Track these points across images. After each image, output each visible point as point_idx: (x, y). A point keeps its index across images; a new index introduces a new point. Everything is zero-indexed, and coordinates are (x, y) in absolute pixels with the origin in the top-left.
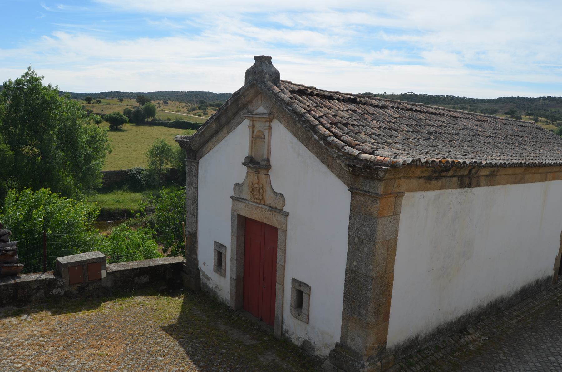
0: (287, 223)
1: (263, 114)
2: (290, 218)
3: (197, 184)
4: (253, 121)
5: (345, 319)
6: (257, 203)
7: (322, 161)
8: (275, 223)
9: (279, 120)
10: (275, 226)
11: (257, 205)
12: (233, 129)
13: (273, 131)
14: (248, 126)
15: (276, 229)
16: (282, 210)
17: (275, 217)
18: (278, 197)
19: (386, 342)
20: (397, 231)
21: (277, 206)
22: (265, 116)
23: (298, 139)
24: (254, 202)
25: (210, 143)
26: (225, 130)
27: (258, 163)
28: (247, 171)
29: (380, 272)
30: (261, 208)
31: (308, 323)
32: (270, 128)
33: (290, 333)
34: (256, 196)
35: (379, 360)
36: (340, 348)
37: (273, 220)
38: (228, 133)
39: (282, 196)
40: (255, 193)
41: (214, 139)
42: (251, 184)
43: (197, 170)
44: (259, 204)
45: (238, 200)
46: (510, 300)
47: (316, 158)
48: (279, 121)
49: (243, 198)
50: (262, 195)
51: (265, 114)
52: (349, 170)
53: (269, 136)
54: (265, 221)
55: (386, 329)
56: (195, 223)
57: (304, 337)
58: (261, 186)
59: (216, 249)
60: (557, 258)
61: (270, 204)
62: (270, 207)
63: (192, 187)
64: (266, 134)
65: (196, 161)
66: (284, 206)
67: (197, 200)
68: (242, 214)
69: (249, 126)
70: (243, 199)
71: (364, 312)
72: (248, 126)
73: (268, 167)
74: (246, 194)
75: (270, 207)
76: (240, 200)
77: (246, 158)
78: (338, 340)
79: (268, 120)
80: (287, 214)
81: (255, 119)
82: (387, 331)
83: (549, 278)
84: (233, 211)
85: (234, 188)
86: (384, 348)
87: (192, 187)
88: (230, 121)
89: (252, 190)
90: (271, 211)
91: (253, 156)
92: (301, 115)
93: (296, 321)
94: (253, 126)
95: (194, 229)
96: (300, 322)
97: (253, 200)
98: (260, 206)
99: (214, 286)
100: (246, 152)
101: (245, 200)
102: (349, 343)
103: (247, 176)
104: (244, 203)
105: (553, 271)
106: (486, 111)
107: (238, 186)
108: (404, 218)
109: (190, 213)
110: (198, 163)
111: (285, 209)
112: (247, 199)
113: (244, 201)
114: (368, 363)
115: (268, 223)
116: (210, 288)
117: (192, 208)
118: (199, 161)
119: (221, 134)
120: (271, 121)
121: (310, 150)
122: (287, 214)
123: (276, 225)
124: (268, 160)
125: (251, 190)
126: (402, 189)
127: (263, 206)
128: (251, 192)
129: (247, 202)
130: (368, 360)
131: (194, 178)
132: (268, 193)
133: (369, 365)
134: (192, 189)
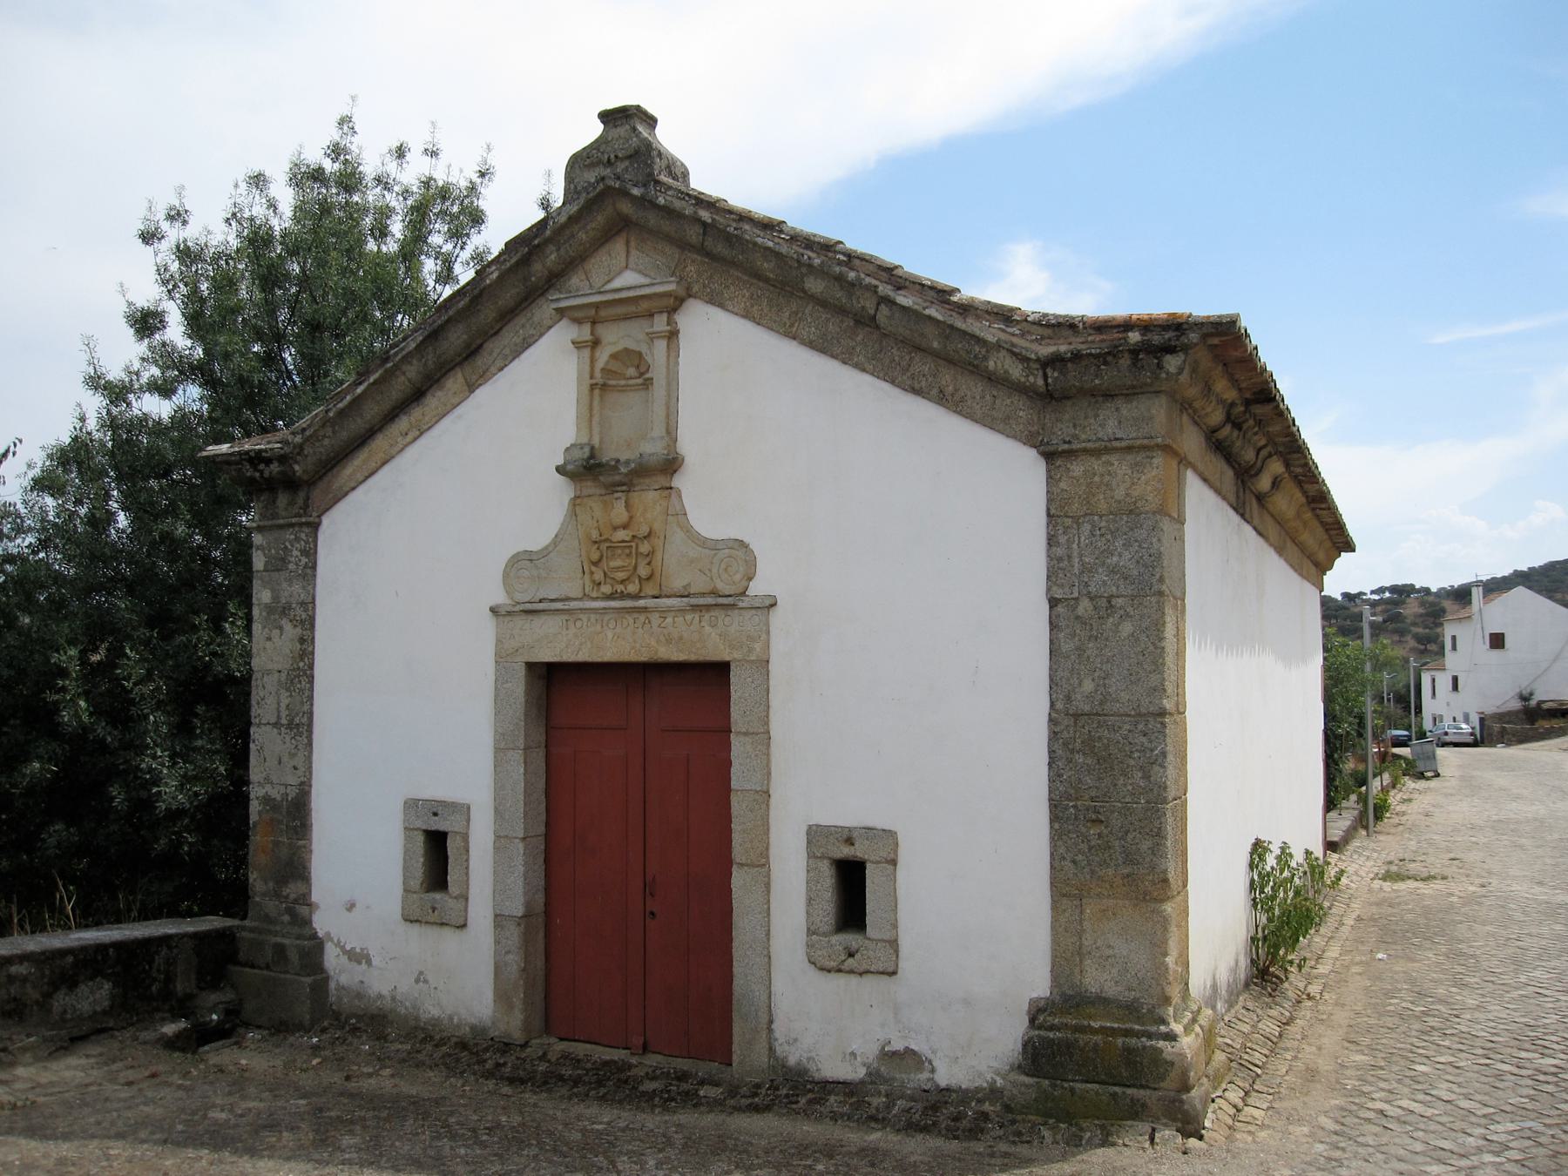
3: (309, 605)
12: (493, 369)
38: (472, 388)
41: (403, 423)
66: (750, 579)
88: (480, 346)
98: (642, 603)
110: (315, 526)
117: (285, 702)
118: (319, 516)
119: (433, 401)
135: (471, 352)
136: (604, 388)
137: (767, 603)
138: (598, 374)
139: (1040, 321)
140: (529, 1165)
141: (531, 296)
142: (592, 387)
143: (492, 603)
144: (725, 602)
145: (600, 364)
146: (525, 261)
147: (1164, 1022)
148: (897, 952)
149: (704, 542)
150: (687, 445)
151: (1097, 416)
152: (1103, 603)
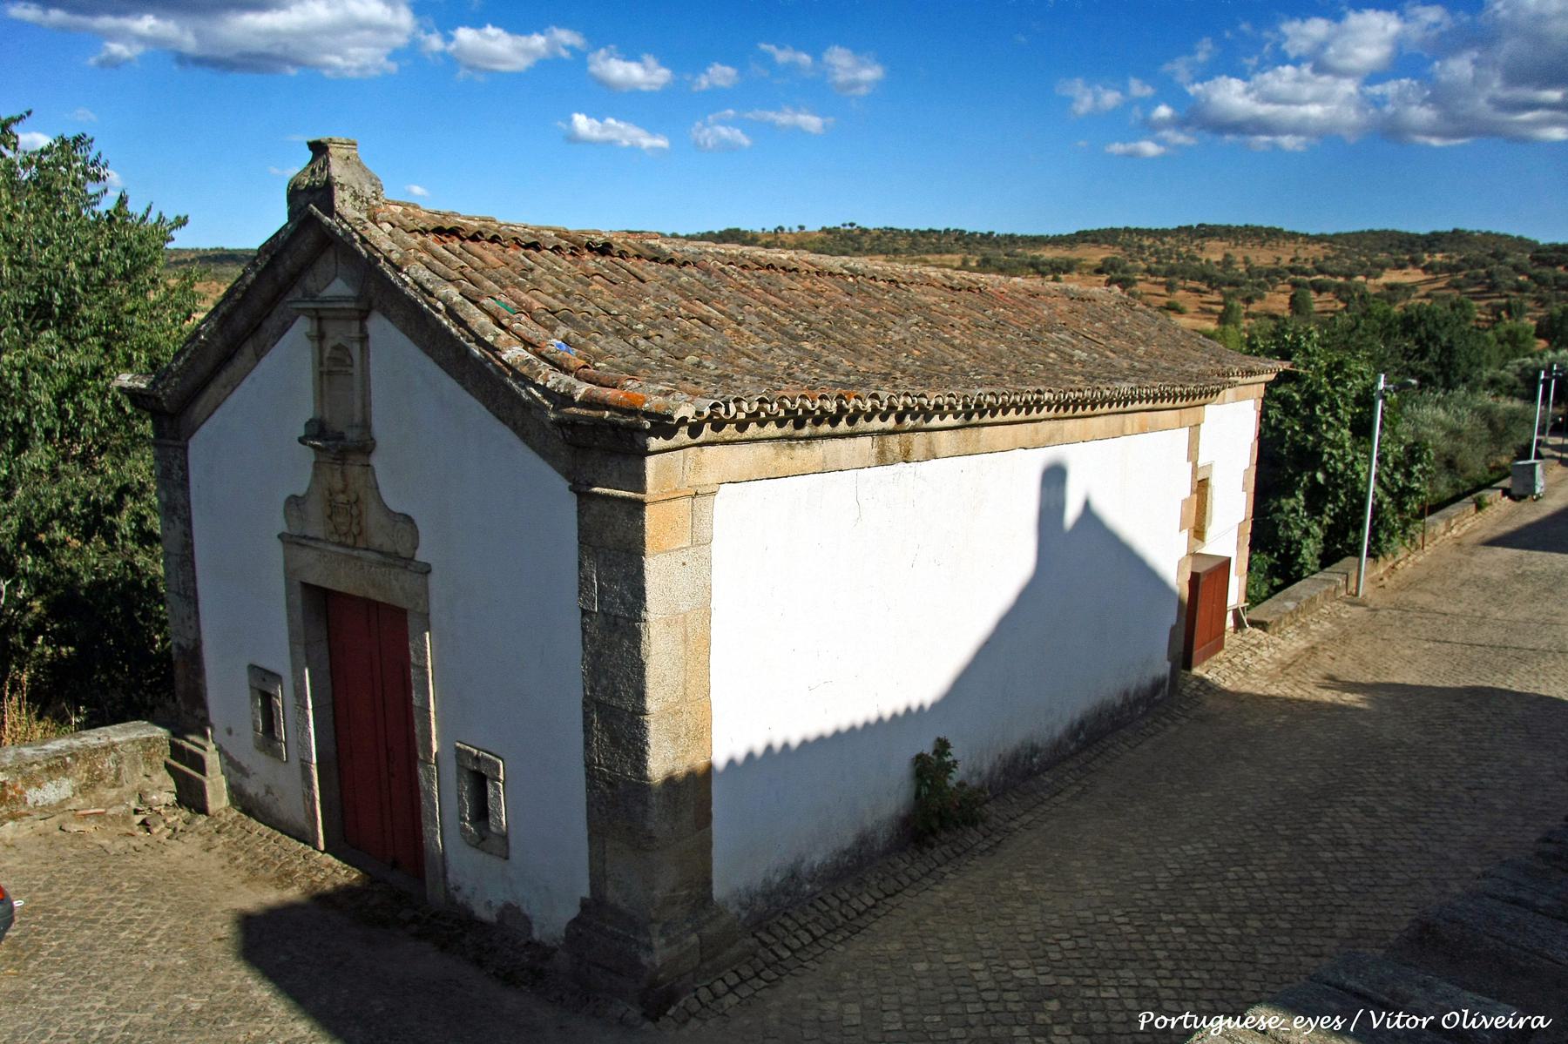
0: (427, 593)
1: (339, 299)
2: (434, 580)
3: (187, 506)
4: (320, 319)
5: (597, 833)
6: (348, 546)
7: (499, 417)
8: (398, 599)
9: (386, 313)
10: (399, 605)
11: (348, 551)
12: (269, 344)
13: (373, 345)
14: (306, 334)
15: (403, 612)
16: (412, 559)
17: (397, 580)
18: (400, 525)
19: (708, 883)
20: (708, 588)
21: (399, 550)
22: (346, 305)
23: (435, 361)
24: (340, 544)
25: (213, 391)
26: (248, 350)
27: (341, 437)
28: (313, 459)
29: (670, 700)
30: (358, 558)
31: (507, 858)
32: (364, 339)
33: (467, 891)
34: (344, 528)
35: (693, 930)
36: (593, 907)
37: (393, 588)
38: (258, 357)
39: (408, 519)
40: (340, 520)
41: (223, 378)
42: (327, 493)
43: (184, 468)
44: (354, 547)
45: (298, 544)
46: (1058, 746)
47: (483, 408)
48: (384, 315)
49: (311, 535)
50: (359, 523)
51: (346, 299)
52: (563, 434)
53: (362, 358)
54: (374, 594)
55: (706, 847)
56: (194, 618)
57: (499, 897)
58: (353, 498)
59: (256, 685)
60: (1173, 629)
61: (381, 545)
62: (381, 553)
63: (175, 518)
64: (356, 349)
65: (180, 443)
66: (416, 548)
67: (192, 554)
68: (312, 581)
69: (309, 337)
70: (311, 539)
71: (639, 808)
72: (306, 334)
73: (366, 448)
74: (316, 529)
75: (381, 553)
76: (304, 541)
77: (307, 425)
78: (585, 892)
79: (356, 314)
80: (426, 570)
81: (322, 314)
82: (710, 853)
83: (1157, 685)
84: (289, 574)
85: (285, 511)
86: (706, 899)
87: (175, 518)
88: (260, 324)
89: (332, 510)
90: (384, 564)
91: (327, 416)
92: (259, 275)
93: (479, 857)
94: (320, 337)
95: (191, 635)
96: (488, 857)
97: (336, 538)
98: (355, 553)
99: (262, 792)
100: (307, 411)
101: (317, 539)
102: (612, 895)
103: (315, 475)
104: (316, 549)
105: (1168, 665)
106: (1232, 289)
107: (294, 502)
108: (722, 550)
109: (178, 594)
110: (185, 449)
111: (421, 556)
112: (321, 536)
113: (312, 543)
114: (663, 941)
115: (380, 599)
116: (250, 797)
117: (181, 578)
118: (187, 441)
119: (239, 363)
120: (364, 316)
121: (467, 389)
122: (426, 570)
123: (402, 603)
124: (366, 425)
125: (328, 512)
126: (709, 477)
127: (362, 553)
128: (330, 517)
129: (321, 545)
130: (662, 933)
131: (179, 493)
132: (373, 518)
133: (669, 944)
134: (177, 522)
135: (255, 328)
136: (330, 373)
137: (426, 569)
138: (326, 362)
139: (1034, 273)
140: (64, 471)
141: (281, 292)
142: (321, 374)
143: (279, 532)
144: (404, 561)
145: (326, 355)
146: (270, 266)
147: (648, 934)
148: (507, 844)
149: (389, 513)
150: (380, 429)
151: (606, 466)
152: (611, 619)
